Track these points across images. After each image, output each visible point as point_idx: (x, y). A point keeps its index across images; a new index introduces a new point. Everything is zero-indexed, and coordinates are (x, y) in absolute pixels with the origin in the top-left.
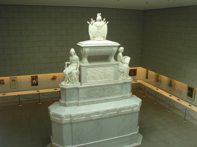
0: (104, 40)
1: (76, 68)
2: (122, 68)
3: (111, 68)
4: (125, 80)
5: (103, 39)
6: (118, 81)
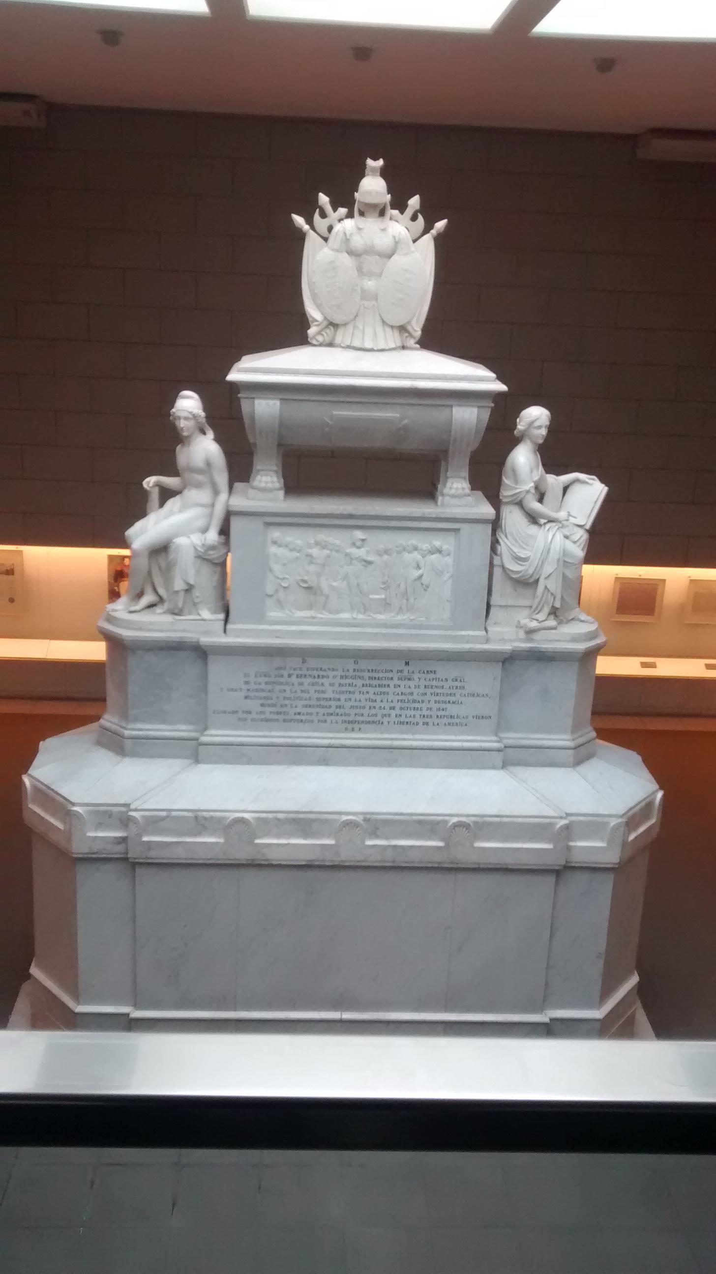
0: (404, 348)
1: (201, 523)
2: (522, 554)
3: (437, 543)
4: (537, 636)
5: (392, 339)
6: (487, 641)
